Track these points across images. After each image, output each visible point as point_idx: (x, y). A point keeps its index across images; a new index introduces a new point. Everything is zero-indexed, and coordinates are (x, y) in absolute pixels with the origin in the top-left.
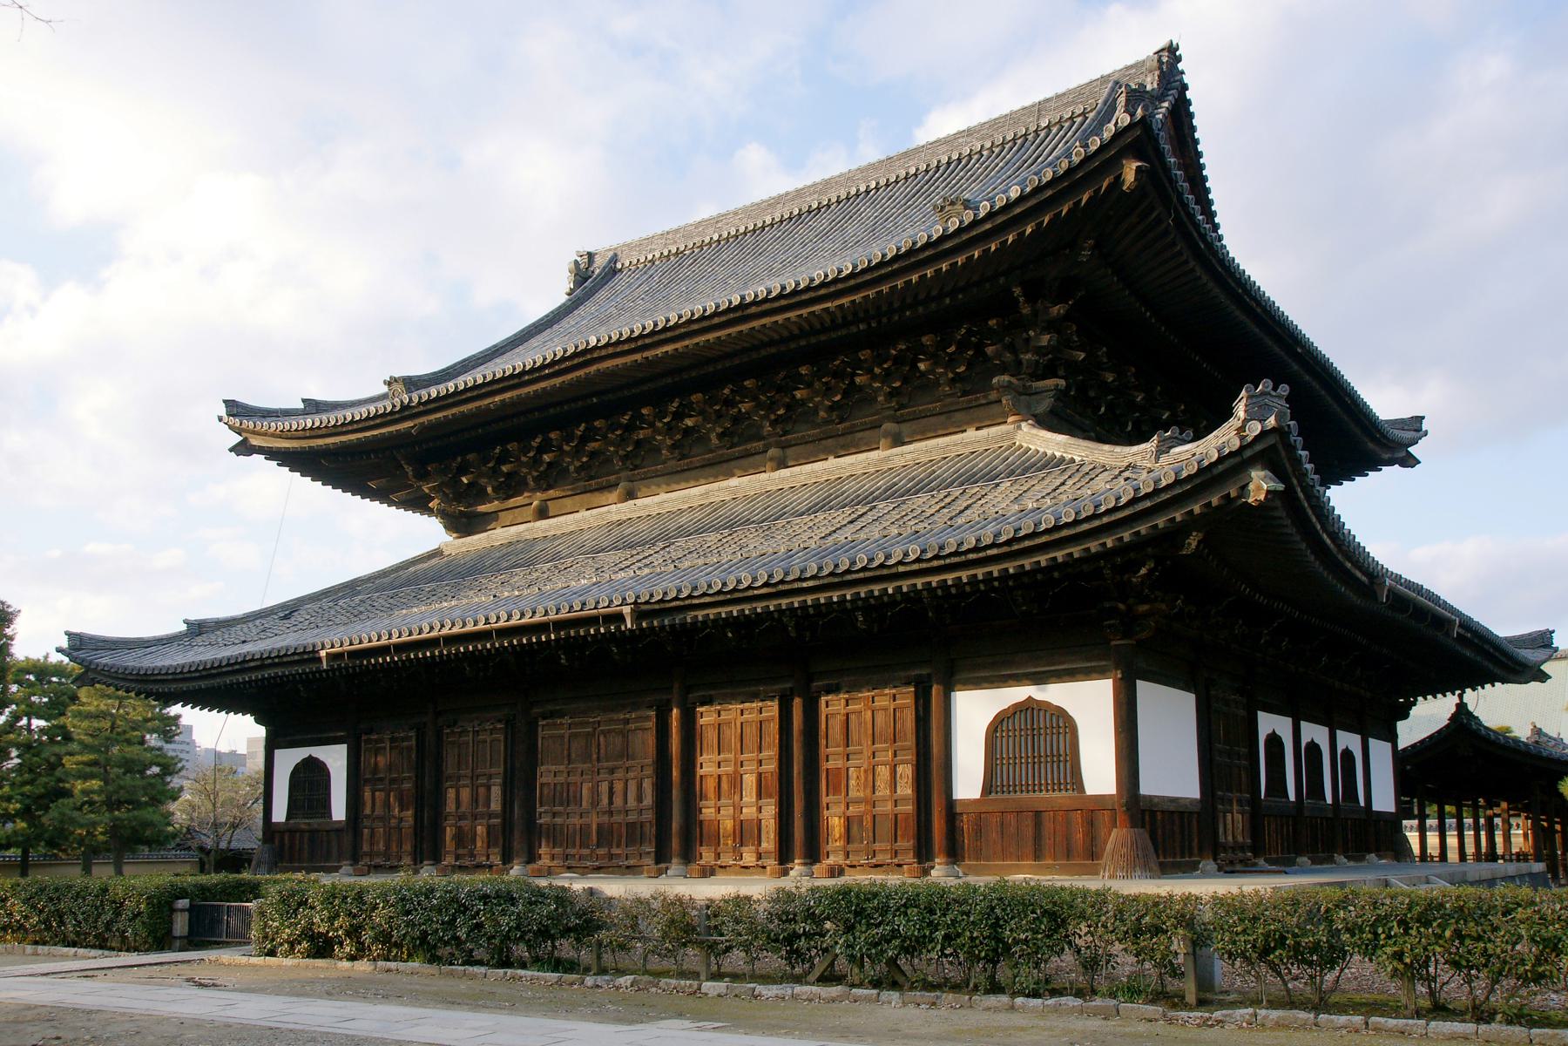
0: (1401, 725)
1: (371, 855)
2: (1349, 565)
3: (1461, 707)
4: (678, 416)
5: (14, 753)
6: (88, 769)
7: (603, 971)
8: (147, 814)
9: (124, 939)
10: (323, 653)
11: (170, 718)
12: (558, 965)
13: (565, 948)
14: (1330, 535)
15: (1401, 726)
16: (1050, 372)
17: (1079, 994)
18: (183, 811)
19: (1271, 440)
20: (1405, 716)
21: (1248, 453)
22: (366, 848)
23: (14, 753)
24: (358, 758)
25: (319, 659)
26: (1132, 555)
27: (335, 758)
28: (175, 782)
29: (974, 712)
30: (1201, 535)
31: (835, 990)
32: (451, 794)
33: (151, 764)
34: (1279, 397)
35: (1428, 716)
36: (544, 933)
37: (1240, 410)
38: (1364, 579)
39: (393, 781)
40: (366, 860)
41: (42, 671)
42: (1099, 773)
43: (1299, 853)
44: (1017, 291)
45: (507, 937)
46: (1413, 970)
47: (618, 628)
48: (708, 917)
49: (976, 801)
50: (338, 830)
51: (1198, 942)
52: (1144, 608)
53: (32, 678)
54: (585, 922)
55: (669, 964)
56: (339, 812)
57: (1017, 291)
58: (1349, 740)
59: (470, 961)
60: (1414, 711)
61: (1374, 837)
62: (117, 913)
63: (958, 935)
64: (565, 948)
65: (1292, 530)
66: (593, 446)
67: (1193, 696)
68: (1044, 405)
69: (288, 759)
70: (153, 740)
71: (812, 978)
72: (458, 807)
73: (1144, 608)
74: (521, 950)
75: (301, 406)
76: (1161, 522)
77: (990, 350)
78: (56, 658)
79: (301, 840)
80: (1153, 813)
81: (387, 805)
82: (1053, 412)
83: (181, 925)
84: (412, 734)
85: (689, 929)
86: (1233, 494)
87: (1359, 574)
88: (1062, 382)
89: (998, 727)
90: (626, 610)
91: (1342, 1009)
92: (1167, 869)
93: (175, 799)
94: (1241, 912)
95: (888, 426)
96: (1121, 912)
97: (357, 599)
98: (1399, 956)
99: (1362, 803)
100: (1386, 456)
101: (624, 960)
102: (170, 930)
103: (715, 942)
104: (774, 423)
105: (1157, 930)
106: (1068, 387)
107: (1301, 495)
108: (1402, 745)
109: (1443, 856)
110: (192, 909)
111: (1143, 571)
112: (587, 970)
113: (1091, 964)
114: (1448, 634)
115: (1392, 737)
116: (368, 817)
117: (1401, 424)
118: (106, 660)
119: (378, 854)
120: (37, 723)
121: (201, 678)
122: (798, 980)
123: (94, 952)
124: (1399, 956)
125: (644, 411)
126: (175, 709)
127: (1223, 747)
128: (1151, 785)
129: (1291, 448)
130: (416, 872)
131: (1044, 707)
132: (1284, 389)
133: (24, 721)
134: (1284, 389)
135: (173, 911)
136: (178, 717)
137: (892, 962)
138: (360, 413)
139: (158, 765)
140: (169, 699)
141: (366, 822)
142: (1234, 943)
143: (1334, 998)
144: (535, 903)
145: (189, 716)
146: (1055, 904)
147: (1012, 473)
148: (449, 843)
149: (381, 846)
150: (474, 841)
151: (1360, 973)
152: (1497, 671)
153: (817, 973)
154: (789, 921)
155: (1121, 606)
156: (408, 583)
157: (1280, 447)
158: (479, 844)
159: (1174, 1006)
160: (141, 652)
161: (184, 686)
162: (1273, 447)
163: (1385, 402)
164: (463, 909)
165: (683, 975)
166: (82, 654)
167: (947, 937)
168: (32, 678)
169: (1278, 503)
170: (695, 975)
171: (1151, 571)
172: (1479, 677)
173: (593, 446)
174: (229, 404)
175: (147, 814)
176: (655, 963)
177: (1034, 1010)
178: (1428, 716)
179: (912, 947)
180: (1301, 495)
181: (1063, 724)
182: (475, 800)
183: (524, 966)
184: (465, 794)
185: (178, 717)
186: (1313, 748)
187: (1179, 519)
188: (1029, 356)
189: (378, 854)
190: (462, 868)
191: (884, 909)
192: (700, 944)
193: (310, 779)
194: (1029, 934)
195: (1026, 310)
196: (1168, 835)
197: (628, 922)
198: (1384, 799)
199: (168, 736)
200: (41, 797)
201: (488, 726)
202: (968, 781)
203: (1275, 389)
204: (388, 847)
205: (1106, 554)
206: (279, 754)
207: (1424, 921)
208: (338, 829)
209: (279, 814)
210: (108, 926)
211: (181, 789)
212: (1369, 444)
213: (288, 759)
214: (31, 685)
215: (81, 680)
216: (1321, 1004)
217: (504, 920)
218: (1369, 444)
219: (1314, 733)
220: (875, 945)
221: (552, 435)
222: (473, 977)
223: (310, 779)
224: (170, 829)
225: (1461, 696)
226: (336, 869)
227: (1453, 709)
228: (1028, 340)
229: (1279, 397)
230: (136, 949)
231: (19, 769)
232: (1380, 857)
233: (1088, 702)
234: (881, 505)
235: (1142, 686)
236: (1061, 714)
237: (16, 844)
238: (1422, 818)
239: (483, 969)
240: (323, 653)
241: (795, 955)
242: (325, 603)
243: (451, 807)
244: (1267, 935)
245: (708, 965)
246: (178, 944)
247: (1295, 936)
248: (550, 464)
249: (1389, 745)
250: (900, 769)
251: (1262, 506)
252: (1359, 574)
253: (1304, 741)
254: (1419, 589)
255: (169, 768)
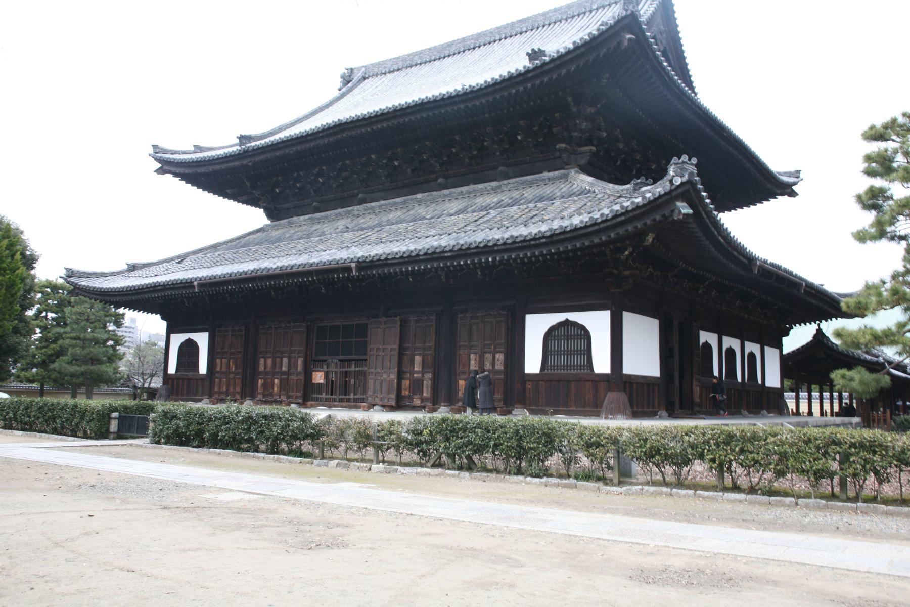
0: (784, 339)
1: (220, 393)
2: (735, 253)
3: (819, 331)
4: (391, 159)
5: (38, 330)
6: (74, 342)
7: (323, 458)
8: (103, 368)
9: (85, 432)
10: (196, 283)
11: (119, 314)
12: (301, 454)
13: (306, 446)
14: (723, 237)
15: (785, 340)
16: (589, 142)
17: (560, 476)
18: (126, 366)
19: (686, 187)
20: (787, 334)
21: (674, 193)
22: (216, 389)
23: (38, 330)
24: (214, 340)
25: (194, 287)
26: (619, 245)
27: (202, 340)
28: (121, 349)
29: (537, 326)
30: (654, 235)
31: (439, 471)
32: (262, 361)
33: (108, 340)
34: (692, 164)
35: (799, 337)
36: (295, 437)
37: (671, 172)
38: (745, 261)
39: (232, 353)
40: (217, 396)
41: (55, 288)
42: (602, 364)
43: (763, 409)
44: (570, 99)
45: (276, 438)
46: (721, 468)
47: (349, 275)
48: (379, 431)
49: (537, 375)
50: (202, 379)
51: (619, 453)
52: (627, 273)
53: (49, 290)
54: (315, 434)
55: (357, 456)
56: (203, 369)
57: (570, 99)
58: (752, 347)
59: (257, 450)
60: (792, 332)
61: (771, 402)
62: (82, 418)
63: (501, 444)
64: (306, 446)
65: (701, 234)
66: (344, 174)
67: (656, 322)
68: (583, 161)
69: (177, 340)
70: (111, 327)
71: (429, 465)
72: (265, 368)
73: (627, 273)
74: (284, 446)
75: (193, 149)
76: (630, 228)
77: (555, 130)
78: (61, 281)
79: (183, 384)
80: (631, 384)
81: (228, 366)
82: (590, 163)
83: (114, 426)
84: (243, 328)
85: (368, 437)
86: (667, 215)
87: (742, 258)
88: (594, 148)
89: (550, 335)
90: (353, 265)
91: (688, 487)
92: (636, 415)
93: (121, 359)
94: (641, 438)
95: (502, 169)
96: (582, 434)
97: (217, 254)
98: (713, 460)
99: (760, 382)
100: (779, 192)
101: (336, 453)
102: (108, 429)
103: (382, 445)
104: (441, 165)
105: (598, 445)
106: (598, 151)
107: (705, 216)
108: (785, 352)
109: (810, 413)
110: (119, 418)
111: (627, 253)
112: (316, 458)
113: (568, 462)
114: (798, 291)
115: (779, 346)
116: (218, 372)
117: (789, 174)
118: (84, 282)
119: (222, 393)
120: (51, 315)
121: (133, 294)
122: (421, 465)
123: (70, 438)
124: (713, 460)
125: (373, 156)
126: (121, 310)
127: (677, 349)
128: (630, 368)
129: (698, 192)
130: (242, 403)
131: (575, 324)
132: (694, 161)
133: (44, 314)
134: (694, 161)
135: (110, 418)
136: (124, 314)
137: (469, 458)
138: (221, 152)
139: (112, 340)
140: (118, 306)
141: (217, 375)
142: (635, 452)
143: (686, 482)
144: (291, 421)
145: (130, 316)
146: (549, 429)
147: (563, 197)
148: (260, 390)
149: (225, 389)
150: (273, 388)
151: (698, 468)
152: (833, 312)
153: (432, 462)
154: (418, 434)
155: (615, 271)
156: (244, 246)
157: (691, 191)
158: (275, 389)
159: (606, 484)
160: (103, 279)
161: (124, 299)
162: (687, 191)
163: (776, 162)
164: (256, 422)
165: (363, 460)
166: (72, 279)
167: (496, 446)
168: (49, 290)
169: (691, 220)
170: (371, 461)
171: (631, 254)
172: (828, 316)
173: (344, 174)
174: (155, 147)
175: (103, 368)
176: (351, 455)
177: (536, 483)
178: (799, 337)
179: (480, 449)
180: (705, 216)
181: (584, 334)
182: (274, 365)
183: (284, 454)
184: (269, 361)
185: (124, 314)
186: (731, 352)
187: (639, 226)
188: (576, 134)
189: (222, 393)
190: (266, 402)
191: (464, 429)
192: (373, 445)
193: (189, 351)
194: (535, 445)
195: (574, 110)
196: (639, 396)
197: (339, 432)
198: (773, 380)
199: (118, 324)
200: (52, 355)
201: (283, 325)
202: (533, 364)
203: (689, 160)
204: (228, 388)
205: (606, 243)
206: (173, 336)
207: (727, 443)
208: (203, 378)
209: (172, 369)
210: (77, 425)
211: (124, 354)
212: (757, 183)
213: (177, 340)
214: (48, 294)
215: (71, 293)
216: (680, 484)
217: (275, 429)
218: (757, 183)
219: (731, 342)
220: (460, 448)
221: (324, 168)
222: (258, 458)
223: (189, 351)
224: (118, 375)
225: (819, 325)
226: (200, 400)
227: (815, 332)
228: (576, 125)
229: (692, 164)
230: (91, 438)
231: (40, 340)
232: (769, 413)
233: (597, 323)
234: (492, 212)
235: (627, 317)
236: (583, 328)
237: (38, 381)
238: (810, 392)
239: (263, 455)
240: (196, 283)
241: (425, 454)
242: (200, 255)
243: (262, 368)
244: (652, 447)
245: (378, 456)
246: (112, 436)
247: (665, 449)
248: (322, 183)
249: (777, 351)
250: (497, 356)
251: (679, 221)
252: (742, 258)
253: (725, 347)
254: (779, 267)
255: (118, 342)
